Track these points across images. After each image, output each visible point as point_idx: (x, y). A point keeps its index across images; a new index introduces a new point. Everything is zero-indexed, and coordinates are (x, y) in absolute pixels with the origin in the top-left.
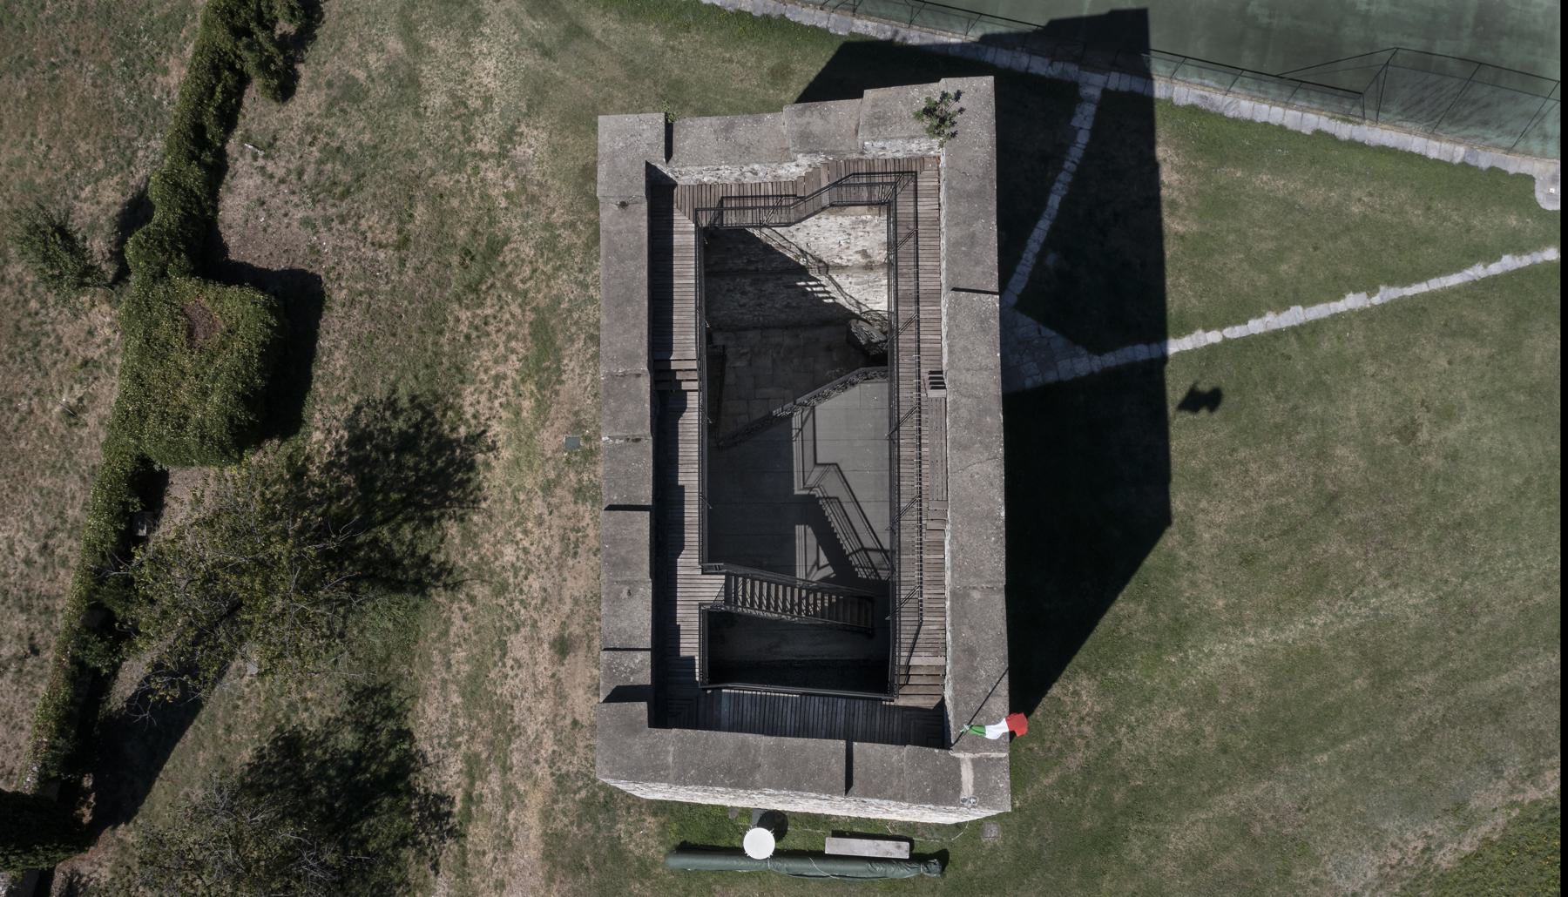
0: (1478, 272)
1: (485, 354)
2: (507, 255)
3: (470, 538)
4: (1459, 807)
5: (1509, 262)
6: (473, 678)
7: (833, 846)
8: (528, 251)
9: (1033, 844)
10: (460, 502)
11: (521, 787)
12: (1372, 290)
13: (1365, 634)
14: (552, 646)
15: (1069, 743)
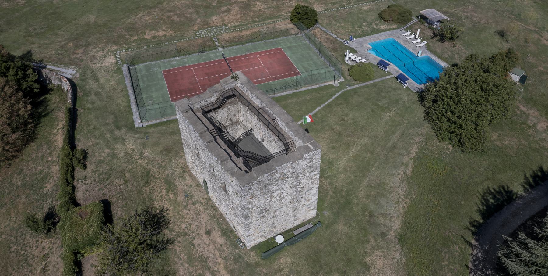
0: (334, 97)
1: (156, 193)
2: (152, 173)
3: (171, 230)
4: (403, 164)
5: (337, 95)
6: (189, 258)
7: (296, 233)
8: (156, 170)
9: (335, 210)
10: (165, 225)
11: (216, 269)
12: (320, 106)
13: (363, 148)
14: (206, 234)
15: (327, 190)
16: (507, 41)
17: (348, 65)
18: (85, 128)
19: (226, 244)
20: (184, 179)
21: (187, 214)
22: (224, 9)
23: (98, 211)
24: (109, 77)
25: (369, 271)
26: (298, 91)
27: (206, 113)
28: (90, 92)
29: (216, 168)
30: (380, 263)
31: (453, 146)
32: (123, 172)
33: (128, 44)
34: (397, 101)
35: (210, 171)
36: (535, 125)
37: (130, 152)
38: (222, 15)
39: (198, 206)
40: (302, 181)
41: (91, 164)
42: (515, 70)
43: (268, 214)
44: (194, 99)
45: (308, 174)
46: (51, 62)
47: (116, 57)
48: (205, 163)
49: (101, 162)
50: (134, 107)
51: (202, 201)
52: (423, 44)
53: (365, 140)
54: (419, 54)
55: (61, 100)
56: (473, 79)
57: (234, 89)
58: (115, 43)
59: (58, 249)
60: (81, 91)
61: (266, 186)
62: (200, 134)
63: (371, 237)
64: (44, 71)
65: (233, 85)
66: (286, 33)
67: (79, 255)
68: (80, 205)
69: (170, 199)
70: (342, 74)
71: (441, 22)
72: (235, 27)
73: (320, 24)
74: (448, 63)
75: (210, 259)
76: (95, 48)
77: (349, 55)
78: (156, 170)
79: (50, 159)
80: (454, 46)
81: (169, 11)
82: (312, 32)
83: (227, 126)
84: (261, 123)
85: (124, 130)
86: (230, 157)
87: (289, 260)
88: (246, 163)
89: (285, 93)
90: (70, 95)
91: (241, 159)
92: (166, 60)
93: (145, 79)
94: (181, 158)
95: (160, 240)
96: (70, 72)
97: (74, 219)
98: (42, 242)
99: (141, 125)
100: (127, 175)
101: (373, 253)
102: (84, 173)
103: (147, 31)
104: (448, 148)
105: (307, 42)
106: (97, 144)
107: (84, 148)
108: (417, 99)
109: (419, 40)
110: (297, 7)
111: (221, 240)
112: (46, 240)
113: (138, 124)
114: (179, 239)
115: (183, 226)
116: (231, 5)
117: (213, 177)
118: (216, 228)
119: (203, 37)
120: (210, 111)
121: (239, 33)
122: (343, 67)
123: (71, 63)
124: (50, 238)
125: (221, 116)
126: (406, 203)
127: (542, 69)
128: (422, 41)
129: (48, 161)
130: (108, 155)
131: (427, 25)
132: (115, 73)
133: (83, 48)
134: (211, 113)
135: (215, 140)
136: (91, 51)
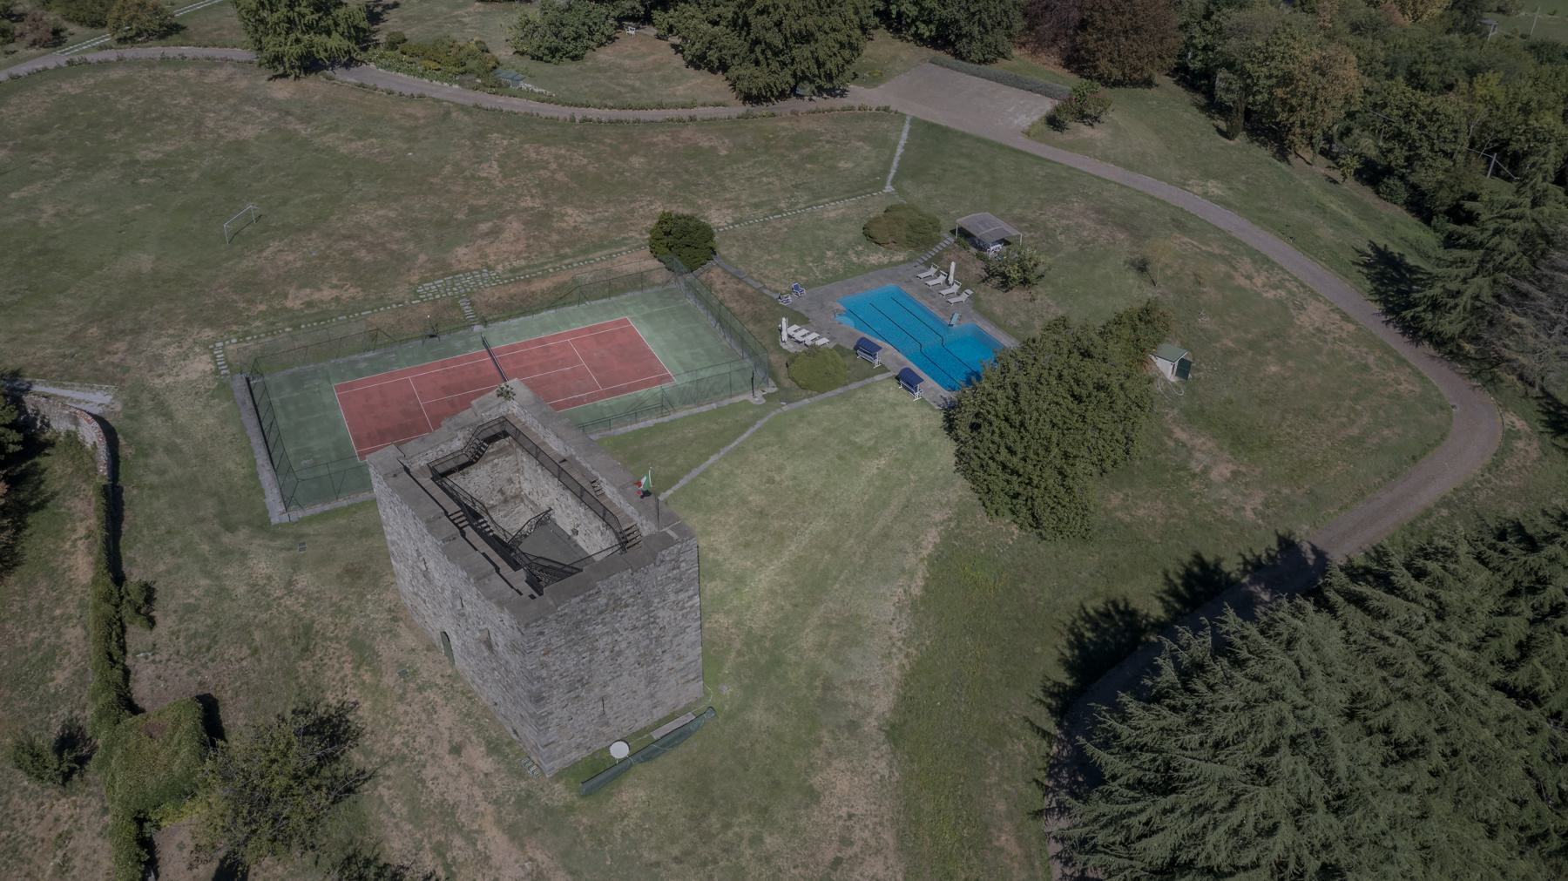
1: (329, 673)
2: (317, 627)
3: (368, 753)
4: (903, 571)
7: (656, 735)
8: (328, 620)
11: (475, 827)
14: (450, 752)
16: (1154, 283)
17: (786, 352)
18: (145, 532)
19: (497, 770)
20: (396, 636)
21: (406, 713)
22: (484, 227)
23: (191, 720)
24: (198, 407)
25: (818, 802)
26: (666, 419)
27: (440, 476)
28: (152, 446)
29: (466, 597)
30: (843, 784)
31: (1021, 527)
32: (245, 629)
33: (244, 324)
34: (896, 433)
35: (454, 606)
36: (1206, 471)
37: (261, 583)
38: (479, 242)
39: (430, 694)
40: (661, 613)
41: (166, 616)
42: (1164, 347)
43: (588, 691)
44: (412, 446)
45: (672, 597)
46: (44, 376)
47: (214, 357)
48: (443, 590)
49: (191, 609)
50: (266, 476)
51: (440, 682)
52: (963, 297)
53: (821, 524)
54: (954, 322)
55: (79, 469)
56: (1055, 373)
57: (504, 420)
58: (209, 323)
59: (93, 819)
60: (129, 445)
61: (577, 624)
62: (428, 521)
63: (824, 733)
64: (29, 400)
65: (502, 411)
66: (638, 281)
67: (147, 825)
68: (143, 711)
69: (364, 683)
70: (772, 375)
71: (1005, 242)
72: (513, 271)
73: (723, 257)
74: (1017, 337)
75: (463, 807)
76: (158, 337)
77: (788, 330)
78: (328, 620)
79: (58, 612)
80: (1033, 300)
81: (346, 237)
82: (703, 277)
83: (493, 507)
84: (568, 493)
85: (243, 533)
86: (497, 570)
87: (641, 794)
88: (534, 582)
89: (635, 427)
90: (102, 455)
91: (522, 574)
92: (341, 361)
93: (291, 408)
94: (387, 588)
95: (340, 773)
96: (99, 399)
97: (133, 741)
98: (52, 806)
99: (285, 518)
100: (258, 636)
101: (829, 764)
102: (150, 637)
103: (292, 291)
104: (1010, 531)
105: (691, 301)
106: (179, 568)
107: (148, 578)
108: (941, 423)
109: (955, 288)
110: (664, 219)
111: (485, 764)
112: (64, 800)
113: (277, 513)
114: (389, 771)
115: (397, 741)
116: (502, 216)
117: (462, 621)
118: (474, 738)
119: (435, 301)
120: (450, 472)
121: (523, 287)
122: (773, 358)
123: (99, 378)
124: (73, 794)
125: (477, 483)
126: (907, 656)
127: (1230, 344)
128: (962, 290)
129: (53, 619)
130: (207, 592)
131: (973, 250)
132: (213, 397)
133: (128, 338)
134: (452, 477)
135: (463, 534)
136: (149, 345)
